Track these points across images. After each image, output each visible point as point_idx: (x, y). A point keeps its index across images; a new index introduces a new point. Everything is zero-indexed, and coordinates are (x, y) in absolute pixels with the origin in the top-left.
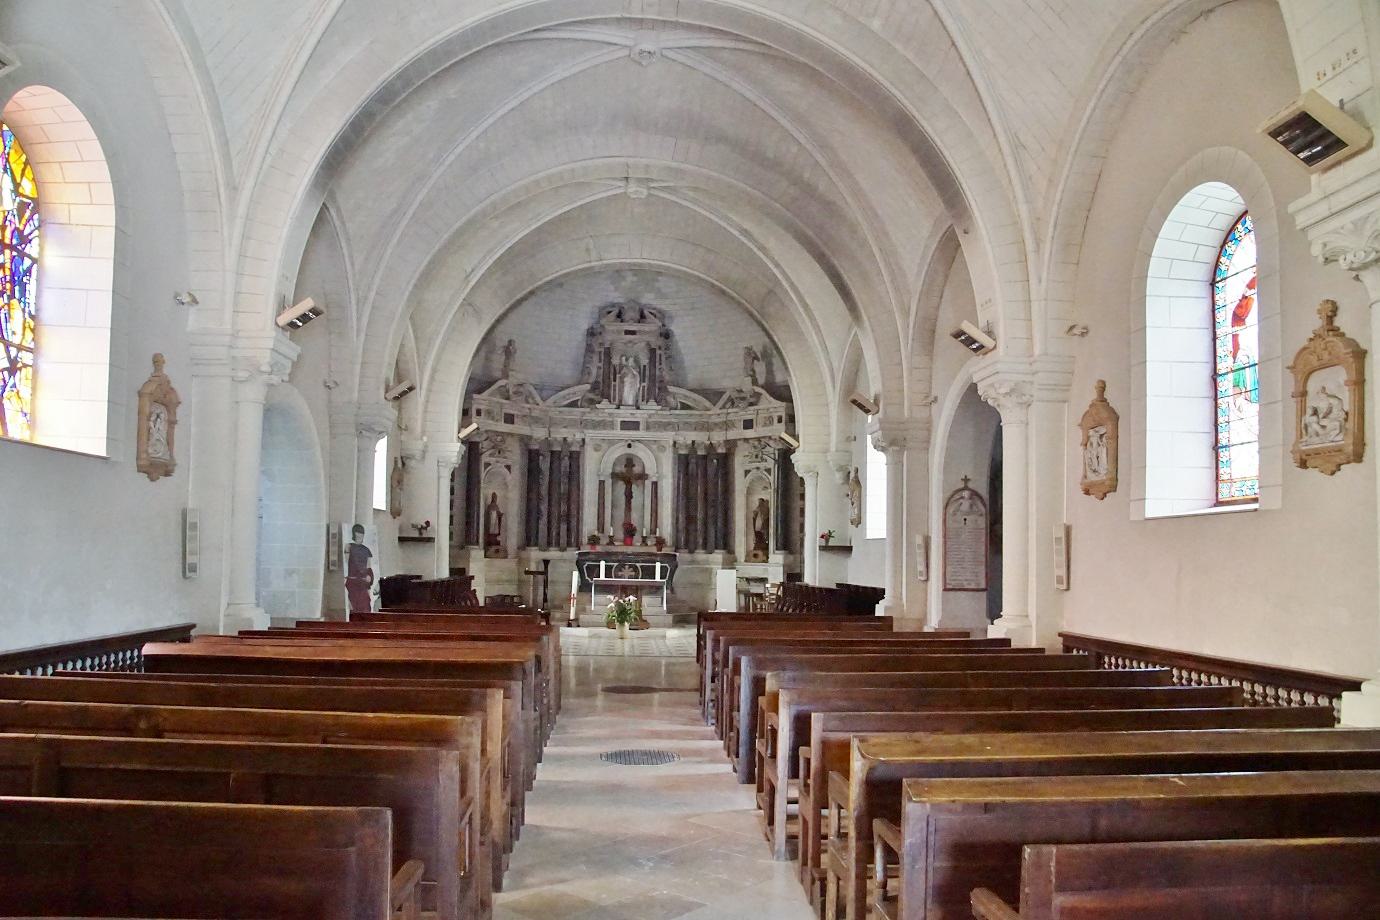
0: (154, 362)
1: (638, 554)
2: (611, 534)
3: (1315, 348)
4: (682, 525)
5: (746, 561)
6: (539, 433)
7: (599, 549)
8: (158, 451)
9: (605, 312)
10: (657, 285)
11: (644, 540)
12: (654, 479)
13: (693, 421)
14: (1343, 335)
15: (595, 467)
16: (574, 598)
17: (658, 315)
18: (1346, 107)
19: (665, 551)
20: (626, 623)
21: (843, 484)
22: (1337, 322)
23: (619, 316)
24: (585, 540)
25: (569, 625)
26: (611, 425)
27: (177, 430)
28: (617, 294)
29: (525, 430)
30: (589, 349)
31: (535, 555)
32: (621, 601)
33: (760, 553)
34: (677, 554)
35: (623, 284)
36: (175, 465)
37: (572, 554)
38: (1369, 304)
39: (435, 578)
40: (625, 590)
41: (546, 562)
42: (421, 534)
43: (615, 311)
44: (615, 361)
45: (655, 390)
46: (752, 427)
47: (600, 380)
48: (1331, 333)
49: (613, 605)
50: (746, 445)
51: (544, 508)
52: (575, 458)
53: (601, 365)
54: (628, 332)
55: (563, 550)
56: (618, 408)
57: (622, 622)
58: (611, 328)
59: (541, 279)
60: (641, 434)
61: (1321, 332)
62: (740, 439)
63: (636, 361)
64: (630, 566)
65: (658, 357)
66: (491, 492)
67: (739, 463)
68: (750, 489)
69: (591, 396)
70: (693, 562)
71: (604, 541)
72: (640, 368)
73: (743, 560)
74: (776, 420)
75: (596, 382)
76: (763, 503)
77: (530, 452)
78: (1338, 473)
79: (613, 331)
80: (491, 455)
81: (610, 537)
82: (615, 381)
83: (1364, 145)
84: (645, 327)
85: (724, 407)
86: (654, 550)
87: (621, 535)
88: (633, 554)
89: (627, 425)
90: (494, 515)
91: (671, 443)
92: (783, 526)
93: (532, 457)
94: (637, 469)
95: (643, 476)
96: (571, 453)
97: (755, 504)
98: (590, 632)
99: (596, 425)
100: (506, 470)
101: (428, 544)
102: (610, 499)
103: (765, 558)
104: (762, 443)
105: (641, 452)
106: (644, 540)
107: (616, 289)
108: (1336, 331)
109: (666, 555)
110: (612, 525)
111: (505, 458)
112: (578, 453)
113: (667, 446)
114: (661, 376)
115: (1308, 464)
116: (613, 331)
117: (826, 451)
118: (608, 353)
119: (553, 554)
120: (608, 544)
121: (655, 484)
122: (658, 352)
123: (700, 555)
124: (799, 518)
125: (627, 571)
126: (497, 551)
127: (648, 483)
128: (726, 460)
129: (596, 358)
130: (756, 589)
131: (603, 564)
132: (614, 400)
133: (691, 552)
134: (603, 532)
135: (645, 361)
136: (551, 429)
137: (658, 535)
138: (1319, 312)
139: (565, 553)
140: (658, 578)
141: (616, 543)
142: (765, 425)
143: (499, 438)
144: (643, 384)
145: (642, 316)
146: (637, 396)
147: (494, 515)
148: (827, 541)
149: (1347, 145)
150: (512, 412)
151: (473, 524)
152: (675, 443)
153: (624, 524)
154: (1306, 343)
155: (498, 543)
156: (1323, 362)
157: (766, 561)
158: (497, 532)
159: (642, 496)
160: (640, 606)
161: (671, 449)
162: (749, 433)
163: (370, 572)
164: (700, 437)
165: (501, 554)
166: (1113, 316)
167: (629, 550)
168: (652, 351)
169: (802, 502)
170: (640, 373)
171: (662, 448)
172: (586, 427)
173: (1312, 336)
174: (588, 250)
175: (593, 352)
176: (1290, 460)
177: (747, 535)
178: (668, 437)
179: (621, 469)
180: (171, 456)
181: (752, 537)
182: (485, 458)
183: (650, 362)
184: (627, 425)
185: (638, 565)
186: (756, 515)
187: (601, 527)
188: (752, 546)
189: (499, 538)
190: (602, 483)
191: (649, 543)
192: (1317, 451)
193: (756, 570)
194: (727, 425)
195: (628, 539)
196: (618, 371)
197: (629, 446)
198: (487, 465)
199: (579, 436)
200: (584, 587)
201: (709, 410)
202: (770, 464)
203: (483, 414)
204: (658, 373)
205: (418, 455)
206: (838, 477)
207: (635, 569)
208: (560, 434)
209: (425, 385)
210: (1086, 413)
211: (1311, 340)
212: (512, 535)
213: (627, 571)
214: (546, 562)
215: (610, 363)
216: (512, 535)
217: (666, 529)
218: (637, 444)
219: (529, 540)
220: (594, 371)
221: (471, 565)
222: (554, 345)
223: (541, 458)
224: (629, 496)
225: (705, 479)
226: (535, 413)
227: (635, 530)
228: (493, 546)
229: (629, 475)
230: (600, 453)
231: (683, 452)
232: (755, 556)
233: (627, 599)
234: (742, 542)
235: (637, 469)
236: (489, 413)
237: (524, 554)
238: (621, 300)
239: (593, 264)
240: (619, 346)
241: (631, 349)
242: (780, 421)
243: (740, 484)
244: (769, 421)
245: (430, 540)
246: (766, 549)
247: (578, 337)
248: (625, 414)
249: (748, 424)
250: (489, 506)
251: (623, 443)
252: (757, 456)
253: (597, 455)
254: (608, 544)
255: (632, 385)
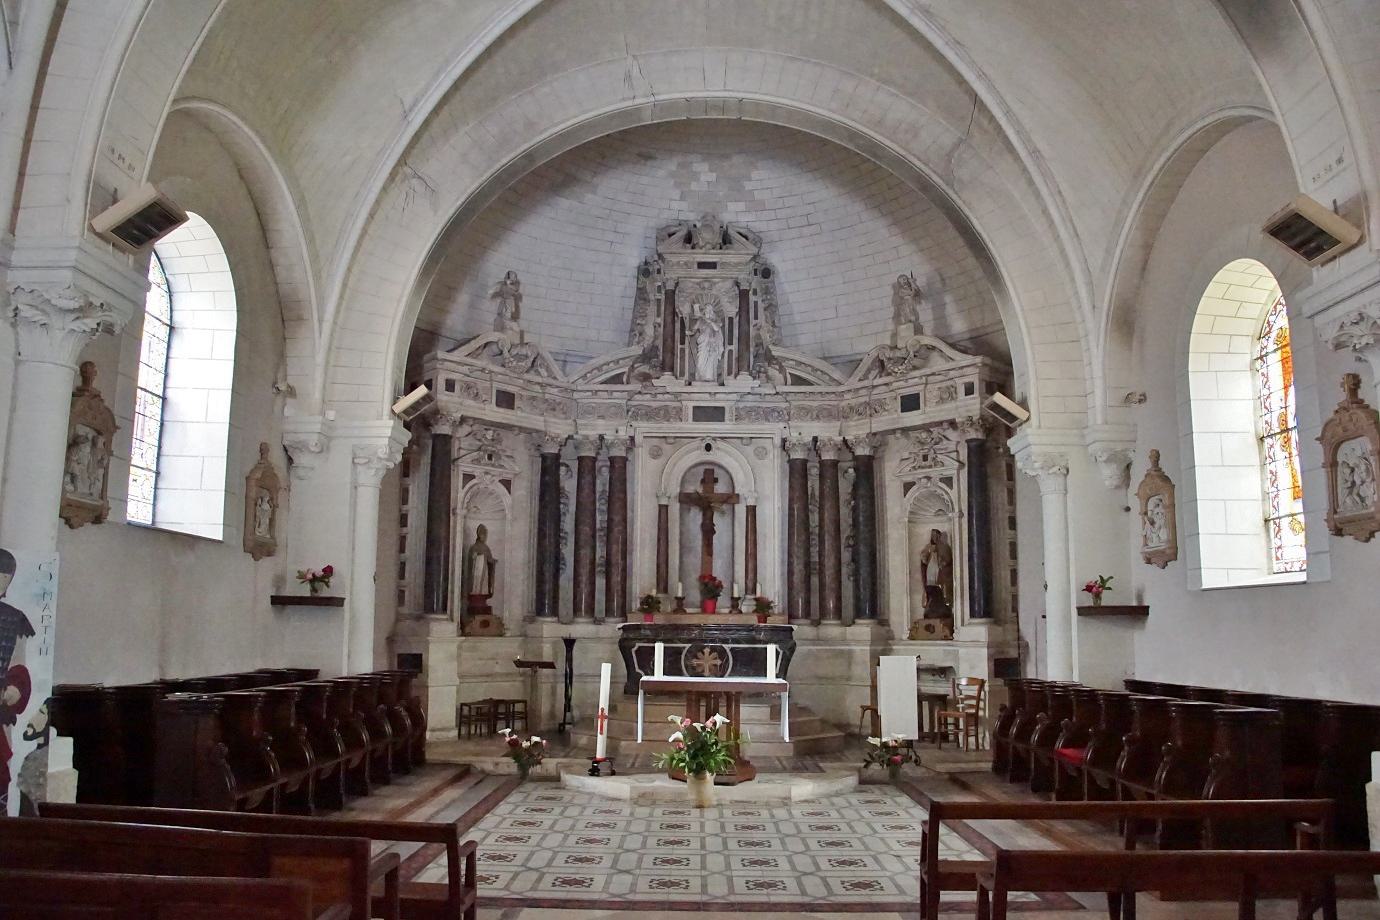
0: (261, 450)
1: (727, 629)
2: (680, 595)
3: (1340, 420)
4: (797, 578)
5: (911, 638)
6: (560, 428)
7: (659, 619)
8: (262, 531)
9: (665, 234)
10: (748, 186)
11: (735, 603)
12: (751, 502)
13: (815, 404)
14: (1367, 407)
15: (651, 485)
16: (603, 717)
17: (750, 236)
18: (1340, 210)
19: (772, 621)
20: (708, 774)
21: (1117, 487)
22: (1361, 395)
23: (689, 239)
24: (636, 605)
25: (594, 772)
26: (679, 414)
27: (278, 511)
28: (684, 205)
29: (536, 421)
30: (641, 295)
31: (550, 630)
32: (698, 726)
33: (937, 623)
34: (795, 627)
35: (694, 186)
36: (109, 509)
37: (613, 628)
38: (1374, 384)
39: (345, 674)
40: (701, 701)
41: (570, 643)
42: (314, 590)
43: (683, 233)
44: (684, 309)
45: (749, 353)
46: (917, 407)
47: (659, 343)
48: (1354, 405)
49: (679, 735)
50: (903, 441)
51: (568, 551)
52: (619, 468)
53: (660, 320)
54: (702, 265)
55: (597, 622)
56: (690, 384)
57: (699, 772)
58: (674, 259)
59: (546, 130)
60: (725, 427)
61: (1346, 405)
62: (894, 431)
63: (719, 313)
64: (713, 649)
65: (752, 305)
66: (474, 525)
67: (892, 473)
68: (917, 514)
69: (645, 369)
70: (817, 640)
71: (667, 606)
72: (723, 321)
73: (905, 636)
74: (961, 390)
75: (654, 348)
76: (937, 536)
77: (544, 457)
78: (1372, 540)
79: (680, 263)
80: (477, 461)
81: (680, 600)
82: (683, 343)
83: (1355, 242)
84: (730, 257)
85: (865, 377)
86: (753, 620)
87: (695, 596)
88: (719, 628)
89: (703, 414)
90: (480, 563)
91: (778, 441)
92: (983, 572)
93: (550, 467)
94: (720, 488)
95: (732, 498)
96: (612, 459)
97: (924, 534)
98: (633, 788)
99: (650, 414)
100: (502, 487)
101: (332, 610)
102: (677, 538)
103: (947, 632)
104: (935, 435)
105: (723, 456)
106: (735, 603)
107: (682, 198)
108: (1360, 403)
109: (775, 629)
110: (680, 580)
111: (502, 466)
112: (625, 460)
113: (769, 447)
114: (758, 337)
115: (1343, 532)
116: (680, 263)
117: (1082, 427)
118: (671, 296)
119: (581, 629)
120: (675, 612)
121: (752, 511)
122: (752, 298)
123: (832, 629)
124: (1011, 562)
125: (708, 660)
126: (485, 624)
127: (741, 511)
128: (867, 470)
129: (652, 309)
130: (941, 688)
131: (659, 647)
132: (682, 374)
133: (817, 623)
134: (666, 590)
135: (731, 309)
136: (579, 422)
137: (758, 595)
138: (1342, 385)
139: (601, 628)
140: (771, 677)
141: (688, 610)
142: (942, 400)
143: (490, 434)
144: (730, 347)
145: (726, 240)
146: (720, 367)
147: (480, 563)
148: (1098, 596)
149: (1340, 242)
150: (510, 389)
151: (433, 575)
152: (784, 441)
153: (702, 578)
154: (1331, 415)
155: (488, 610)
156: (1348, 434)
157: (949, 635)
158: (485, 591)
159: (729, 531)
160: (737, 736)
161: (778, 451)
162: (913, 418)
163: (21, 678)
164: (828, 431)
165: (492, 628)
166: (1160, 391)
167: (711, 620)
168: (743, 295)
169: (1013, 532)
170: (723, 327)
171: (761, 453)
172: (635, 417)
173: (1337, 408)
174: (628, 77)
175: (646, 301)
176: (1141, 557)
177: (911, 592)
178: (775, 429)
179: (695, 487)
180: (272, 537)
181: (920, 596)
182: (464, 466)
183: (739, 313)
184: (703, 414)
185: (727, 647)
186: (928, 557)
187: (662, 582)
188: (921, 612)
189: (489, 602)
190: (663, 510)
191: (744, 609)
192: (1341, 521)
193: (935, 653)
194: (872, 409)
195: (709, 603)
196: (687, 325)
197: (708, 448)
198: (468, 477)
199: (623, 434)
200: (629, 687)
201: (840, 384)
202: (950, 468)
203: (457, 387)
204: (753, 332)
205: (313, 440)
206: (1109, 474)
207: (722, 654)
208: (593, 428)
209: (329, 315)
210: (1142, 483)
211: (1337, 412)
212: (514, 591)
213: (708, 660)
214: (570, 643)
215: (674, 313)
216: (514, 591)
217: (772, 584)
218: (720, 444)
219: (545, 603)
220: (649, 331)
221: (432, 647)
222: (576, 273)
223: (563, 469)
224: (708, 531)
225: (837, 501)
226: (553, 393)
227: (719, 586)
228: (478, 615)
229: (707, 497)
230: (661, 460)
231: (798, 455)
232: (929, 628)
233: (709, 723)
234: (902, 600)
235: (720, 488)
236: (469, 388)
237: (531, 629)
238: (692, 217)
239: (638, 101)
240: (688, 285)
241: (710, 300)
242: (969, 390)
243: (894, 507)
244: (950, 394)
245: (338, 602)
246: (947, 617)
247: (624, 282)
248: (702, 394)
249: (910, 403)
250: (472, 550)
251: (696, 443)
252: (925, 458)
253: (653, 464)
254: (675, 612)
255: (712, 348)
